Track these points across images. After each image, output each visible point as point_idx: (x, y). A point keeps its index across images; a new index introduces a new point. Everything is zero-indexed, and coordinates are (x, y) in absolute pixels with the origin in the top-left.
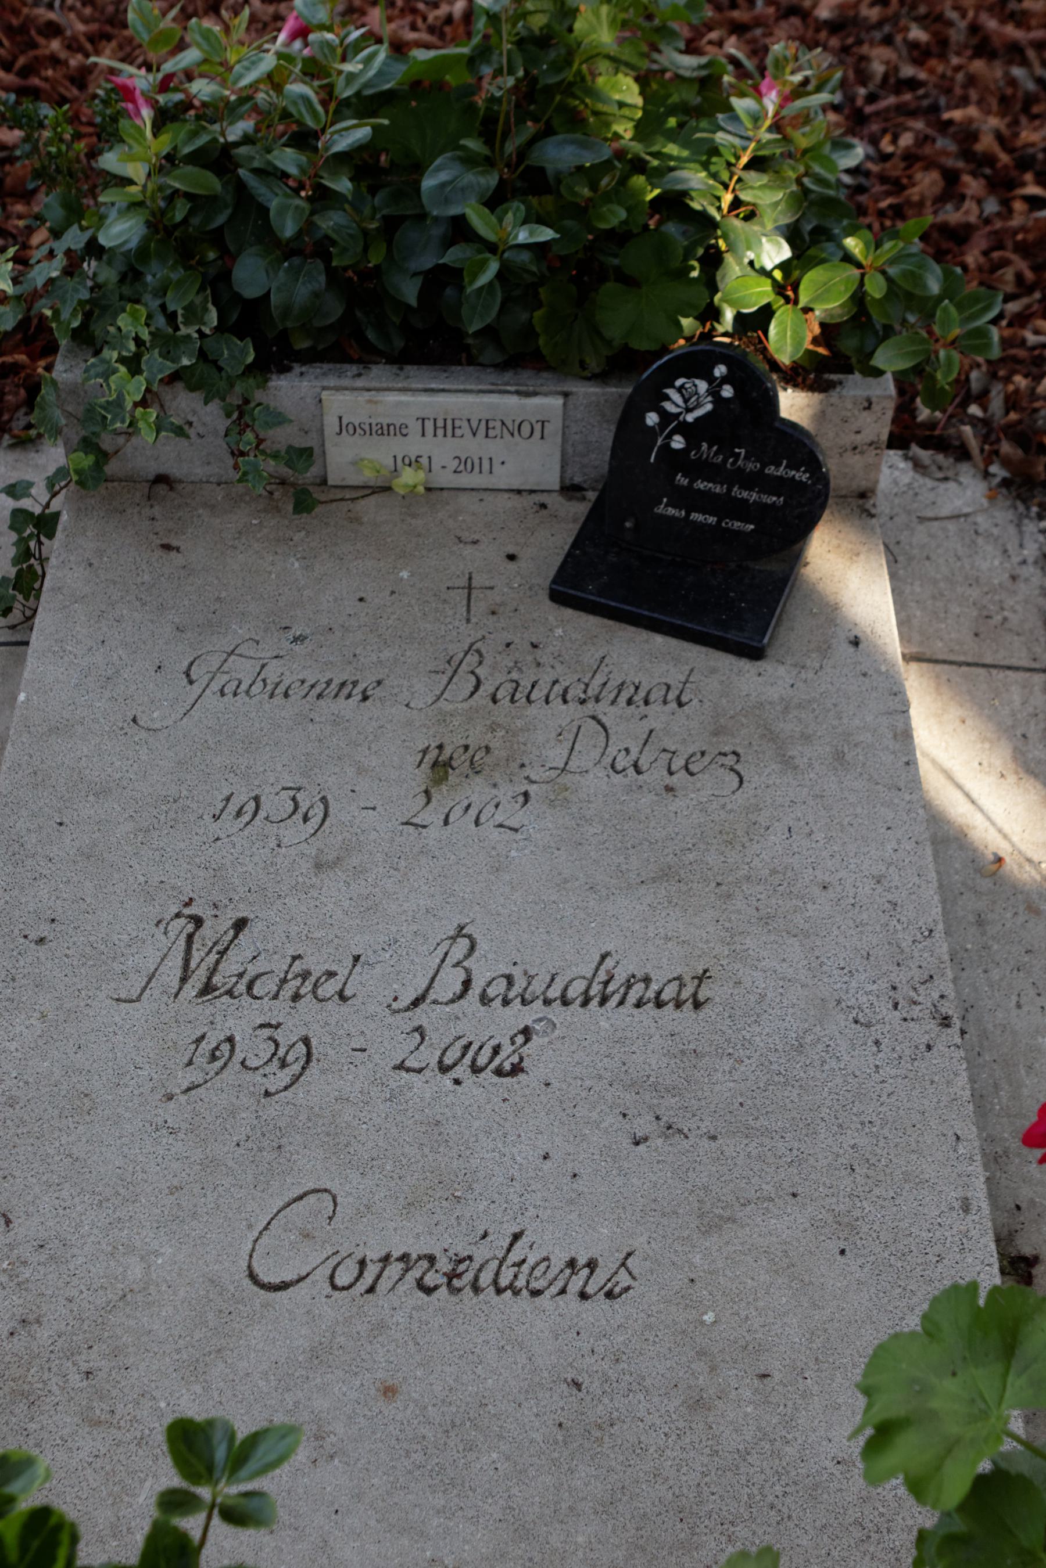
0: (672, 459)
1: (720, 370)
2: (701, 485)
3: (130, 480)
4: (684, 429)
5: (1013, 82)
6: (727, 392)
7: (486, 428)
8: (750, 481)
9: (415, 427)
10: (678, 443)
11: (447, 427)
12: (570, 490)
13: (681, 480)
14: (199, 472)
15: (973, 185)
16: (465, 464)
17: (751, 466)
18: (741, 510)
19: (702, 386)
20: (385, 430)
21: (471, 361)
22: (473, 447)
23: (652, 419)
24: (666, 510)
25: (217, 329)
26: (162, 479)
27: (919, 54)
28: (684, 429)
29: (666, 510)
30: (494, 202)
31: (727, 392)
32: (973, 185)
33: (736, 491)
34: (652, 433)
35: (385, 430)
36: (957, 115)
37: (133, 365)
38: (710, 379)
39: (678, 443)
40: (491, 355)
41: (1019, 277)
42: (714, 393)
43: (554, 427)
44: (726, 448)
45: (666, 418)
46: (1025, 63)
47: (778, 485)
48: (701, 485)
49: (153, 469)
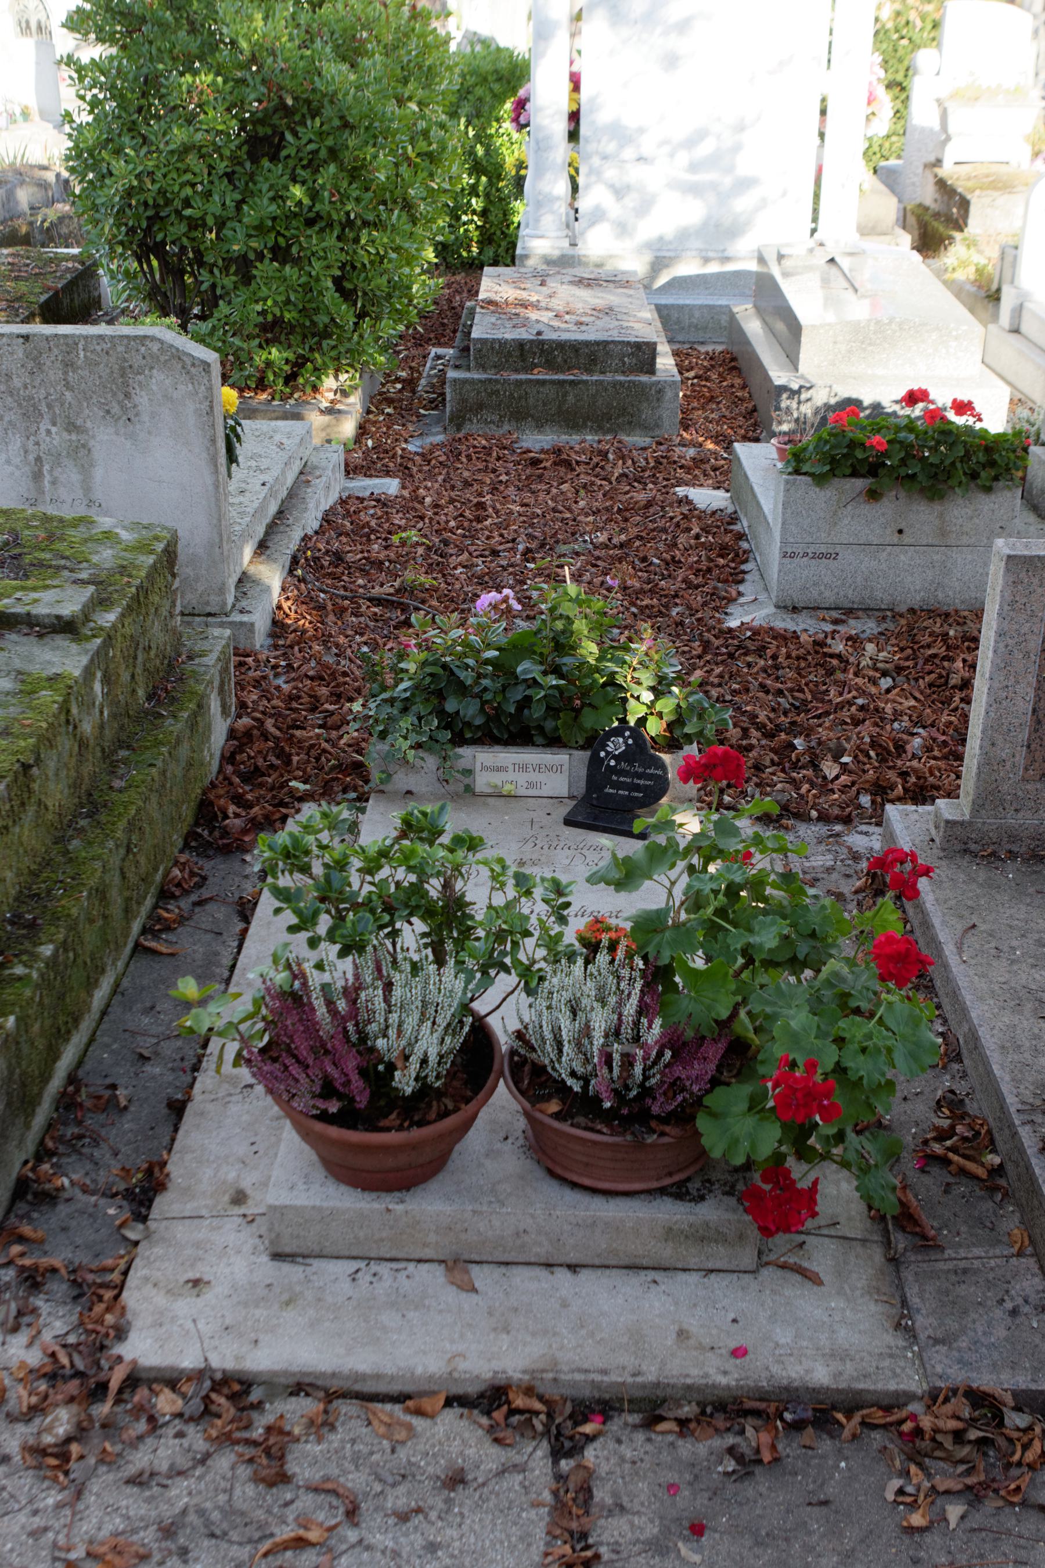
0: (611, 770)
1: (627, 734)
2: (622, 779)
3: (396, 793)
4: (615, 757)
5: (779, 704)
6: (630, 741)
7: (539, 768)
8: (640, 776)
9: (511, 767)
10: (613, 763)
11: (524, 768)
12: (571, 797)
13: (614, 778)
14: (424, 789)
15: (754, 733)
16: (531, 785)
17: (641, 770)
18: (637, 788)
19: (621, 740)
20: (499, 769)
21: (534, 745)
22: (534, 777)
23: (602, 754)
24: (609, 790)
25: (438, 728)
26: (409, 792)
27: (734, 692)
28: (615, 757)
29: (609, 790)
30: (545, 673)
31: (630, 741)
32: (754, 733)
33: (636, 781)
34: (602, 760)
35: (499, 769)
36: (748, 708)
37: (406, 738)
38: (623, 737)
39: (613, 763)
40: (539, 740)
41: (772, 761)
42: (625, 742)
43: (566, 767)
44: (630, 762)
45: (608, 753)
46: (784, 696)
47: (651, 777)
48: (622, 779)
49: (406, 788)
